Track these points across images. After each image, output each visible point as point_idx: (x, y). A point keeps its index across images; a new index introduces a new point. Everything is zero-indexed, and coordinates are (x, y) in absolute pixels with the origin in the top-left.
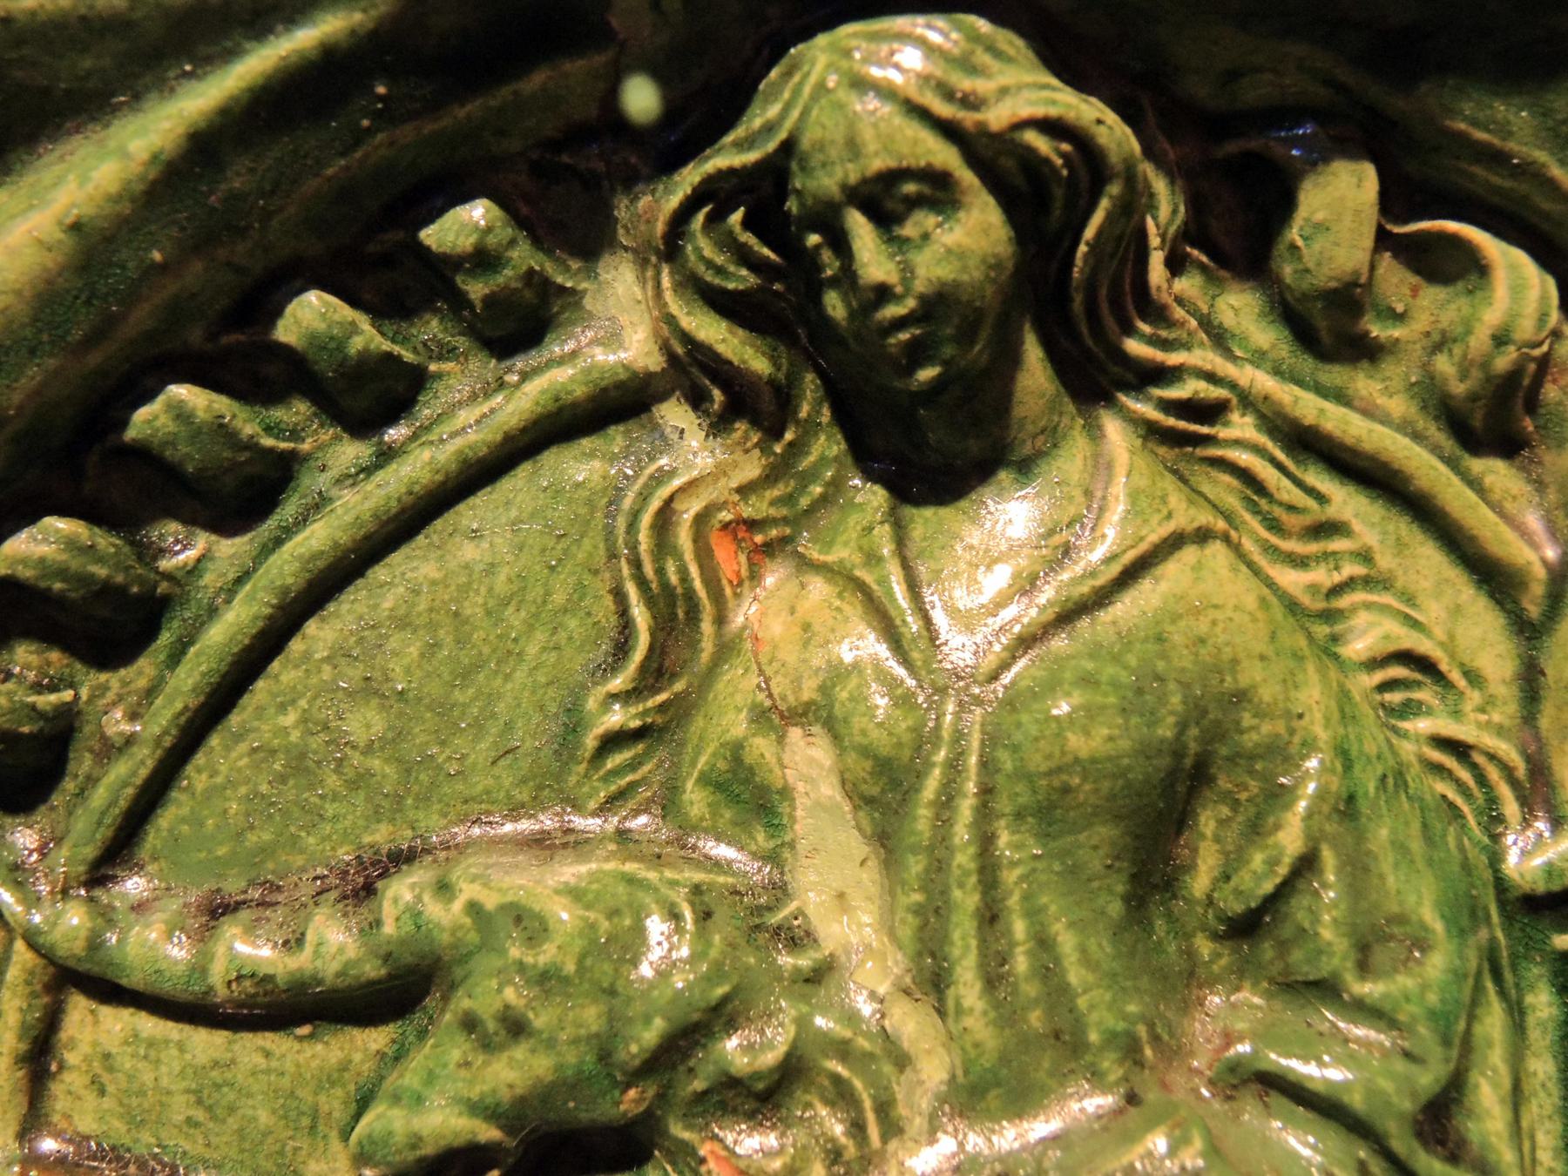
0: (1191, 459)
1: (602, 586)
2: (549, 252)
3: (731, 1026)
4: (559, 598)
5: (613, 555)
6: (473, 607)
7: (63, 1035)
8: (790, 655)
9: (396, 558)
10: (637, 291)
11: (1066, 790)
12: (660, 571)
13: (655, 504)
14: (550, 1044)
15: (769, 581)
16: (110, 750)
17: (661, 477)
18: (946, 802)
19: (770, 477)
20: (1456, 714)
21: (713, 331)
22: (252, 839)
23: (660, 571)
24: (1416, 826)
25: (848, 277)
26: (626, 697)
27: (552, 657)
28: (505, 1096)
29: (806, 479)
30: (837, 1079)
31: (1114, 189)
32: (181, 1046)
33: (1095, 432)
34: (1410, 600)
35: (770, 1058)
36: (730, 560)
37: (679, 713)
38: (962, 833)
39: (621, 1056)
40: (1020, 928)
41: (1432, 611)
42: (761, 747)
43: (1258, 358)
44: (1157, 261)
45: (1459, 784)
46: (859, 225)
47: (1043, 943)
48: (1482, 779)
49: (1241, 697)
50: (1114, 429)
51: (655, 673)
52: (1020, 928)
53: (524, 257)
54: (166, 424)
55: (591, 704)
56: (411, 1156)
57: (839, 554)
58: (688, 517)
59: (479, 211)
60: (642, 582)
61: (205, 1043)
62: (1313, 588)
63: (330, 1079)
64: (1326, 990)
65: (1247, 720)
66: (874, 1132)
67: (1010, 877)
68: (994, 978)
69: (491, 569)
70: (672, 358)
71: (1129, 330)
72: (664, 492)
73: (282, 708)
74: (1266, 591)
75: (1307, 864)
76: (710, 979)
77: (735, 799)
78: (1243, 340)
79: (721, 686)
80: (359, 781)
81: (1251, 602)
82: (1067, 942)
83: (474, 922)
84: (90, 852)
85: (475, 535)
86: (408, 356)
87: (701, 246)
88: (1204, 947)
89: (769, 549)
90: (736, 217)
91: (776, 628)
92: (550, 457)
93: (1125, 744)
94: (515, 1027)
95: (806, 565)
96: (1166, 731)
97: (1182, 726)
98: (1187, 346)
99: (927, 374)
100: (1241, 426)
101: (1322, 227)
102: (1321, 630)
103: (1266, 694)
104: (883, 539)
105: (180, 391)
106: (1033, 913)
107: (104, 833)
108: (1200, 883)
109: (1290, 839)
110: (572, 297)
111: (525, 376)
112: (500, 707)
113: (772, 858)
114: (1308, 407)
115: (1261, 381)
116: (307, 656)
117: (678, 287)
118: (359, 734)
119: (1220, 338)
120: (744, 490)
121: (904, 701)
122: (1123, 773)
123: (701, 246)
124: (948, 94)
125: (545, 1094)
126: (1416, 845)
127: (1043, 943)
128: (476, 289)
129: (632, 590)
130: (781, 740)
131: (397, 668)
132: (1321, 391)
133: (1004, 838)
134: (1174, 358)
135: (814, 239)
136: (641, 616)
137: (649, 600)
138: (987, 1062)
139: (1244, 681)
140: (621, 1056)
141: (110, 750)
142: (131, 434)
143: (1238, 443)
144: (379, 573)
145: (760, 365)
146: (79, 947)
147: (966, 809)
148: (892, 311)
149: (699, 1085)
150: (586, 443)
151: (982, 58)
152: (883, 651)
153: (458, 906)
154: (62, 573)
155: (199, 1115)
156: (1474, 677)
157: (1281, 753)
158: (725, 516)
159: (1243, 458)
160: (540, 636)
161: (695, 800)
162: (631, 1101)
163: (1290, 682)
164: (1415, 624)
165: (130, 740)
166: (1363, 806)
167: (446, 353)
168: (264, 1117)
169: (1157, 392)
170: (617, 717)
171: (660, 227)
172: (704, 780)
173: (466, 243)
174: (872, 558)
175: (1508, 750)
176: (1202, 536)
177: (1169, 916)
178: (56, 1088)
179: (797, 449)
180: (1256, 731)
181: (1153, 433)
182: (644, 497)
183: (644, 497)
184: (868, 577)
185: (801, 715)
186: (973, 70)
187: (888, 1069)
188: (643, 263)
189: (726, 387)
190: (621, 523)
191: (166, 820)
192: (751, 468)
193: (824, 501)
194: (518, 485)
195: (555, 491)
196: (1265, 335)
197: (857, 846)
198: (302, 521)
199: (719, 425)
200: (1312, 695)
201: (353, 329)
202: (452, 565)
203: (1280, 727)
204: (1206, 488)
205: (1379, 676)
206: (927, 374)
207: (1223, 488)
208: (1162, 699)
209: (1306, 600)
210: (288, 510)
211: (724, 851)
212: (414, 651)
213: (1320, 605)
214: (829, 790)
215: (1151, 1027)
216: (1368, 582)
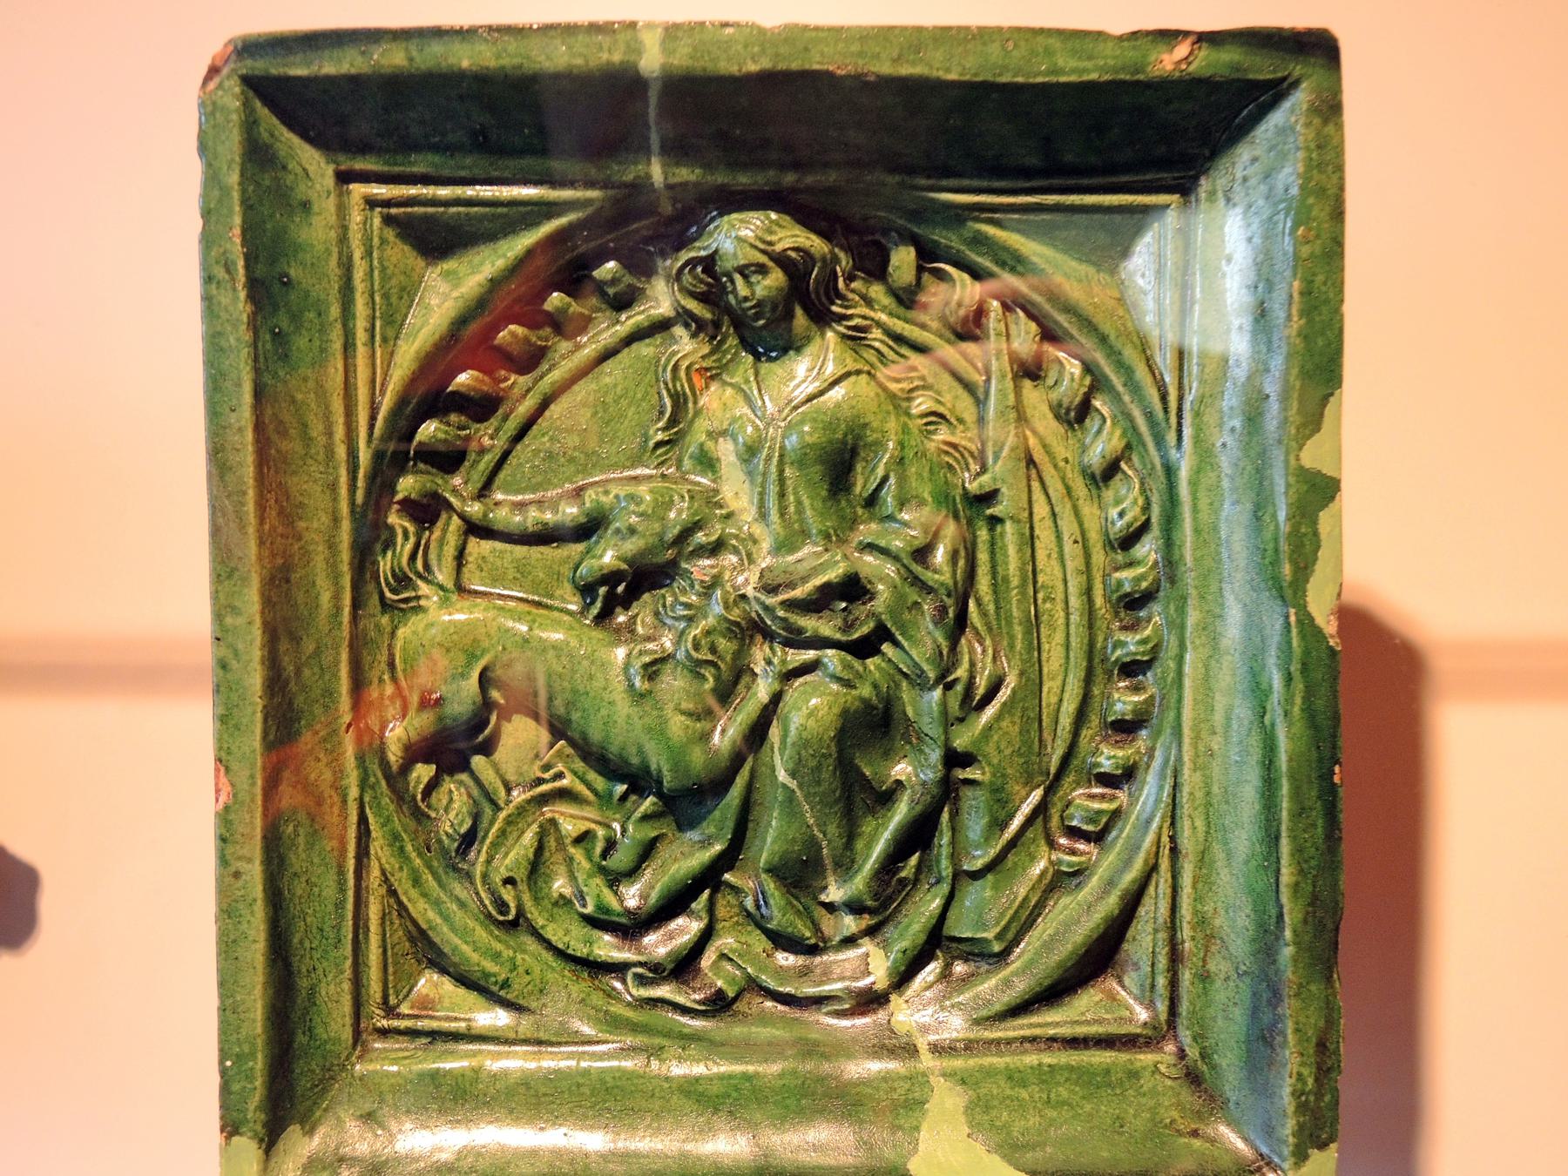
0: (860, 345)
1: (653, 391)
2: (635, 276)
3: (701, 528)
4: (639, 396)
5: (657, 380)
6: (609, 399)
7: (467, 551)
8: (719, 414)
9: (581, 382)
10: (665, 289)
11: (806, 454)
12: (674, 386)
13: (672, 363)
14: (644, 536)
15: (712, 389)
16: (482, 451)
17: (674, 353)
18: (769, 458)
19: (712, 353)
20: (953, 434)
21: (692, 305)
22: (533, 480)
23: (674, 386)
24: (927, 469)
25: (734, 291)
26: (664, 429)
27: (636, 417)
28: (629, 554)
29: (725, 352)
30: (734, 546)
31: (819, 265)
32: (511, 552)
33: (823, 335)
34: (939, 393)
35: (713, 538)
36: (699, 382)
37: (681, 435)
38: (773, 469)
39: (666, 539)
40: (792, 498)
41: (947, 398)
42: (710, 444)
43: (884, 309)
44: (841, 281)
45: (956, 459)
46: (738, 278)
47: (799, 503)
48: (962, 455)
49: (865, 425)
50: (830, 334)
51: (673, 421)
52: (792, 498)
53: (628, 279)
54: (508, 338)
55: (651, 432)
56: (599, 574)
57: (736, 379)
58: (684, 367)
59: (611, 264)
60: (668, 390)
61: (520, 551)
62: (902, 390)
63: (564, 561)
64: (890, 518)
65: (868, 433)
66: (746, 562)
67: (789, 482)
68: (783, 512)
69: (615, 386)
70: (678, 313)
71: (833, 303)
72: (676, 358)
73: (543, 435)
74: (880, 391)
75: (885, 479)
76: (694, 515)
77: (701, 463)
78: (878, 302)
79: (696, 424)
80: (572, 460)
81: (872, 394)
82: (806, 502)
83: (900, 174)
84: (479, 485)
85: (610, 374)
86: (587, 312)
87: (687, 278)
88: (860, 511)
89: (712, 378)
90: (699, 269)
91: (715, 405)
92: (635, 346)
93: (824, 439)
94: (632, 531)
95: (725, 383)
96: (839, 436)
97: (845, 435)
98: (855, 307)
99: (761, 322)
100: (876, 333)
101: (898, 267)
102: (905, 404)
103: (875, 425)
104: (751, 372)
105: (512, 327)
106: (796, 493)
107: (484, 479)
108: (858, 489)
109: (880, 472)
110: (643, 290)
111: (628, 318)
112: (620, 434)
113: (714, 481)
114: (899, 326)
115: (883, 317)
116: (551, 417)
117: (680, 290)
118: (571, 444)
119: (868, 302)
120: (703, 357)
121: (756, 428)
122: (824, 448)
123: (687, 278)
124: (764, 242)
125: (643, 553)
126: (926, 474)
127: (799, 503)
128: (611, 291)
129: (664, 393)
130: (716, 442)
131: (583, 420)
132: (907, 321)
133: (787, 470)
134: (850, 312)
135: (724, 279)
136: (668, 402)
137: (671, 396)
138: (781, 539)
139: (867, 421)
140: (666, 539)
141: (482, 451)
142: (496, 342)
143: (875, 339)
144: (576, 388)
145: (708, 316)
146: (480, 515)
147: (775, 460)
148: (748, 304)
149: (691, 549)
150: (647, 341)
151: (775, 228)
152: (749, 412)
153: (611, 496)
154: (474, 389)
155: (519, 576)
156: (961, 421)
157: (879, 445)
158: (697, 366)
159: (877, 344)
160: (633, 409)
161: (687, 463)
162: (670, 554)
163: (884, 421)
164: (940, 402)
165: (493, 446)
166: (906, 461)
167: (599, 310)
168: (541, 575)
169: (845, 323)
170: (660, 436)
171: (674, 272)
172: (691, 457)
173: (609, 277)
174: (747, 381)
175: (973, 448)
176: (858, 372)
177: (848, 501)
178: (465, 570)
179: (721, 342)
180: (871, 437)
181: (844, 337)
182: (668, 360)
183: (668, 360)
184: (745, 387)
185: (724, 433)
186: (771, 233)
187: (750, 543)
188: (668, 282)
189: (696, 323)
190: (660, 369)
191: (502, 475)
192: (706, 349)
193: (731, 360)
194: (625, 356)
195: (638, 358)
196: (886, 300)
197: (742, 477)
198: (550, 370)
199: (694, 336)
200: (892, 425)
201: (569, 305)
202: (601, 384)
203: (880, 435)
204: (865, 355)
205: (925, 420)
206: (761, 322)
207: (870, 355)
208: (839, 425)
209: (900, 394)
210: (545, 366)
211: (698, 479)
212: (589, 415)
213: (906, 396)
214: (733, 458)
215: (835, 531)
216: (924, 387)
